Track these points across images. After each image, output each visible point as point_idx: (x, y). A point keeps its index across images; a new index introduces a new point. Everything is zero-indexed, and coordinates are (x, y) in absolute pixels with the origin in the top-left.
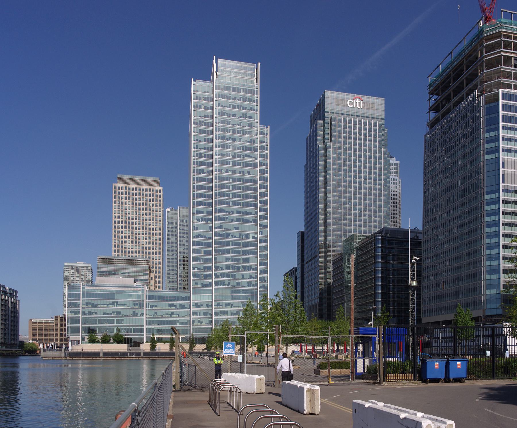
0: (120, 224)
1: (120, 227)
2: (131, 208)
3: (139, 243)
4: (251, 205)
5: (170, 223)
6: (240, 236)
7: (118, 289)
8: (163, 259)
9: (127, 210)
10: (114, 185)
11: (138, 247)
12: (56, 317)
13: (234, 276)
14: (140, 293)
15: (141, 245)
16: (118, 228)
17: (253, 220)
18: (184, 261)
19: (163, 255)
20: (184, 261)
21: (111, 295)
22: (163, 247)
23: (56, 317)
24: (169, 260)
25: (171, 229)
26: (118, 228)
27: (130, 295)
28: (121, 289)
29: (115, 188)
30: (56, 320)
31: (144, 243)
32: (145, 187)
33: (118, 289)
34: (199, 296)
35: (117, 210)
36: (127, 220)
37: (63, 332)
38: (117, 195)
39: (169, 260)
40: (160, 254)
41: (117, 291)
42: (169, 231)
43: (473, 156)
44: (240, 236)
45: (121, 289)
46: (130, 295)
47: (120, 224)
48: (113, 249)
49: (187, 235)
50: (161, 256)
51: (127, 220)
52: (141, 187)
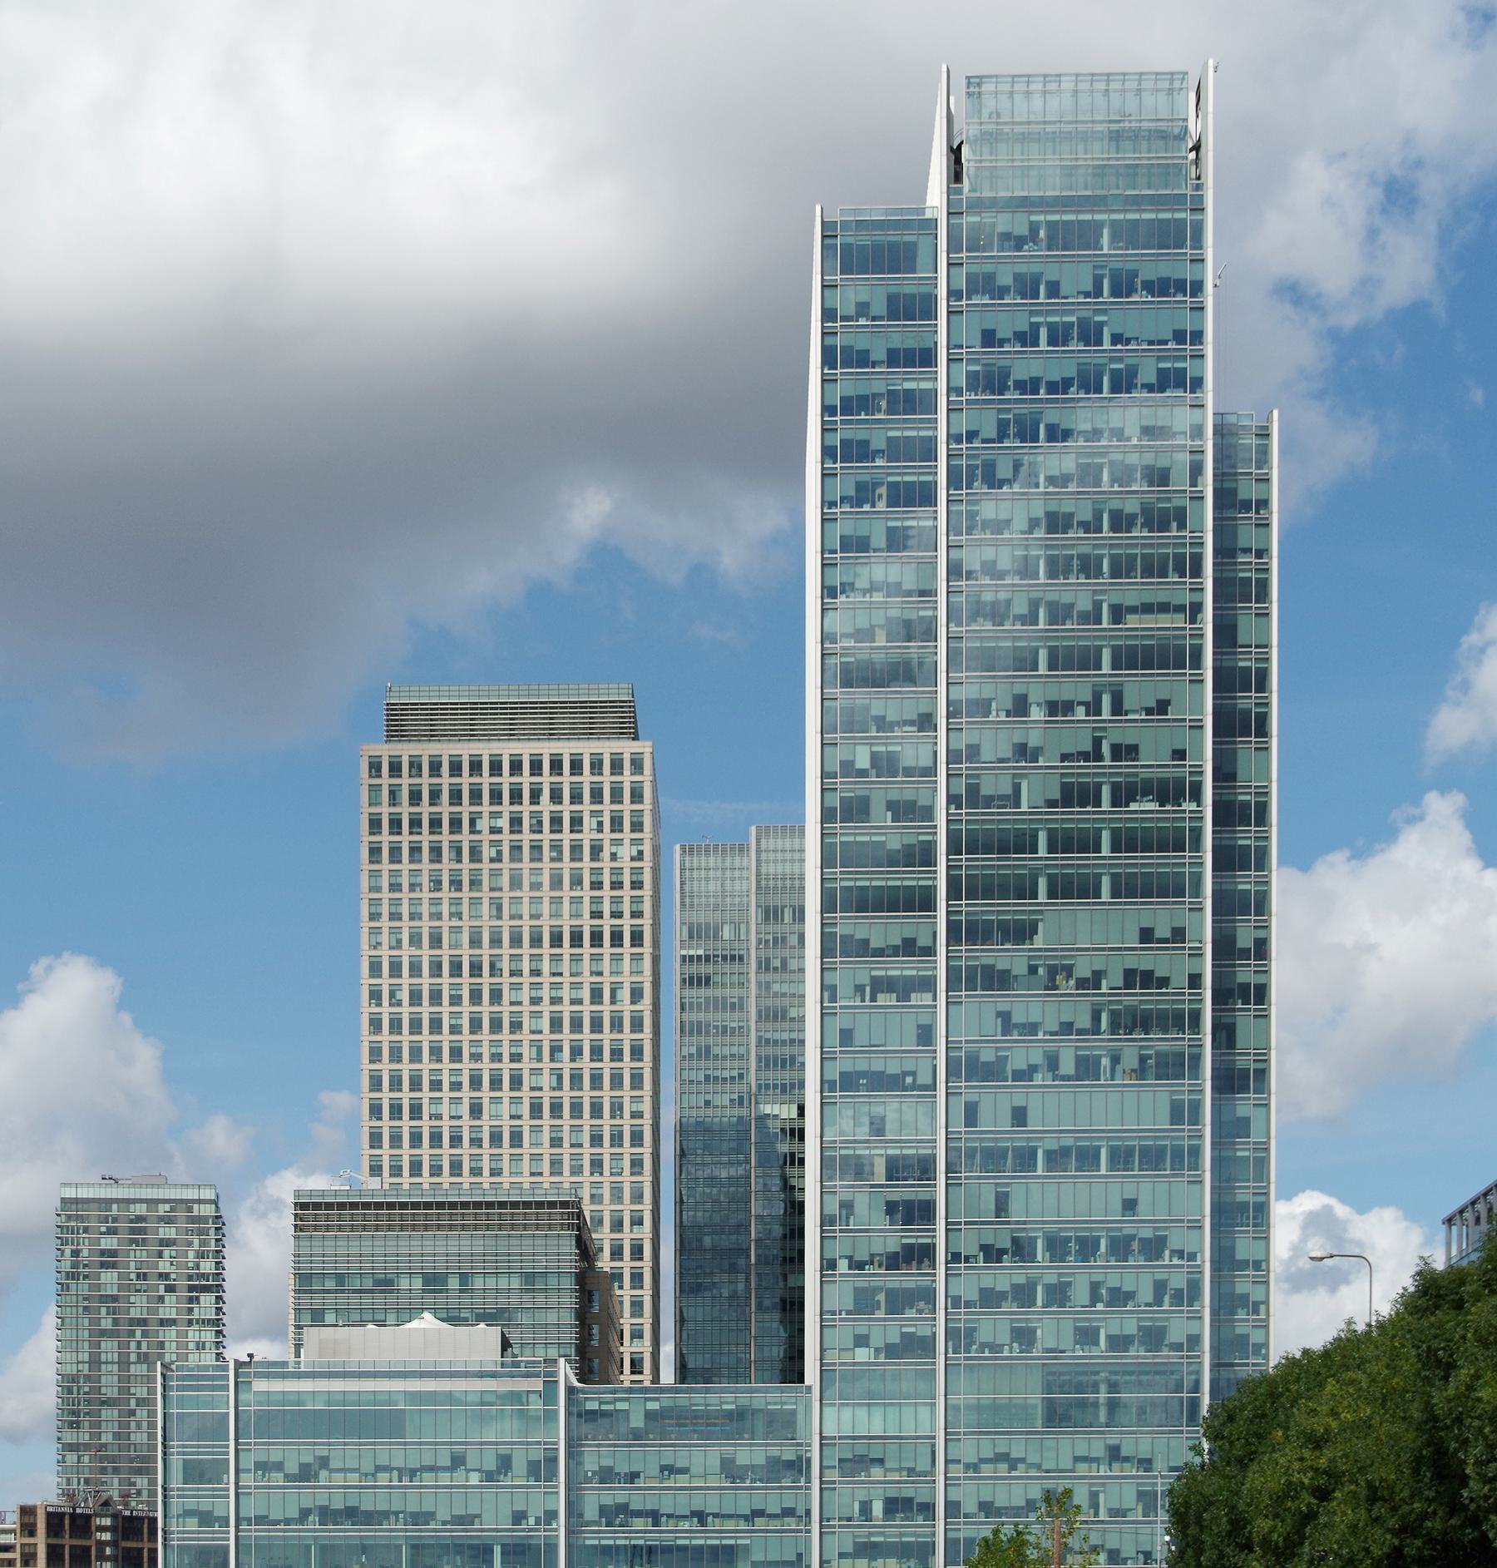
0: (406, 980)
1: (404, 996)
3: (516, 1082)
5: (694, 933)
6: (1096, 1018)
8: (656, 960)
11: (505, 1109)
12: (27, 1512)
15: (525, 1093)
16: (395, 1002)
17: (1179, 560)
18: (775, 1065)
19: (656, 944)
20: (775, 1065)
22: (656, 926)
23: (27, 1512)
24: (695, 969)
25: (703, 969)
26: (395, 1002)
28: (429, 1385)
29: (375, 767)
30: (29, 1529)
31: (546, 1080)
32: (546, 749)
35: (386, 895)
37: (67, 1541)
38: (385, 1037)
39: (695, 969)
40: (637, 938)
42: (691, 981)
44: (1096, 1018)
45: (429, 1385)
47: (406, 980)
48: (367, 1009)
50: (647, 949)
52: (525, 749)
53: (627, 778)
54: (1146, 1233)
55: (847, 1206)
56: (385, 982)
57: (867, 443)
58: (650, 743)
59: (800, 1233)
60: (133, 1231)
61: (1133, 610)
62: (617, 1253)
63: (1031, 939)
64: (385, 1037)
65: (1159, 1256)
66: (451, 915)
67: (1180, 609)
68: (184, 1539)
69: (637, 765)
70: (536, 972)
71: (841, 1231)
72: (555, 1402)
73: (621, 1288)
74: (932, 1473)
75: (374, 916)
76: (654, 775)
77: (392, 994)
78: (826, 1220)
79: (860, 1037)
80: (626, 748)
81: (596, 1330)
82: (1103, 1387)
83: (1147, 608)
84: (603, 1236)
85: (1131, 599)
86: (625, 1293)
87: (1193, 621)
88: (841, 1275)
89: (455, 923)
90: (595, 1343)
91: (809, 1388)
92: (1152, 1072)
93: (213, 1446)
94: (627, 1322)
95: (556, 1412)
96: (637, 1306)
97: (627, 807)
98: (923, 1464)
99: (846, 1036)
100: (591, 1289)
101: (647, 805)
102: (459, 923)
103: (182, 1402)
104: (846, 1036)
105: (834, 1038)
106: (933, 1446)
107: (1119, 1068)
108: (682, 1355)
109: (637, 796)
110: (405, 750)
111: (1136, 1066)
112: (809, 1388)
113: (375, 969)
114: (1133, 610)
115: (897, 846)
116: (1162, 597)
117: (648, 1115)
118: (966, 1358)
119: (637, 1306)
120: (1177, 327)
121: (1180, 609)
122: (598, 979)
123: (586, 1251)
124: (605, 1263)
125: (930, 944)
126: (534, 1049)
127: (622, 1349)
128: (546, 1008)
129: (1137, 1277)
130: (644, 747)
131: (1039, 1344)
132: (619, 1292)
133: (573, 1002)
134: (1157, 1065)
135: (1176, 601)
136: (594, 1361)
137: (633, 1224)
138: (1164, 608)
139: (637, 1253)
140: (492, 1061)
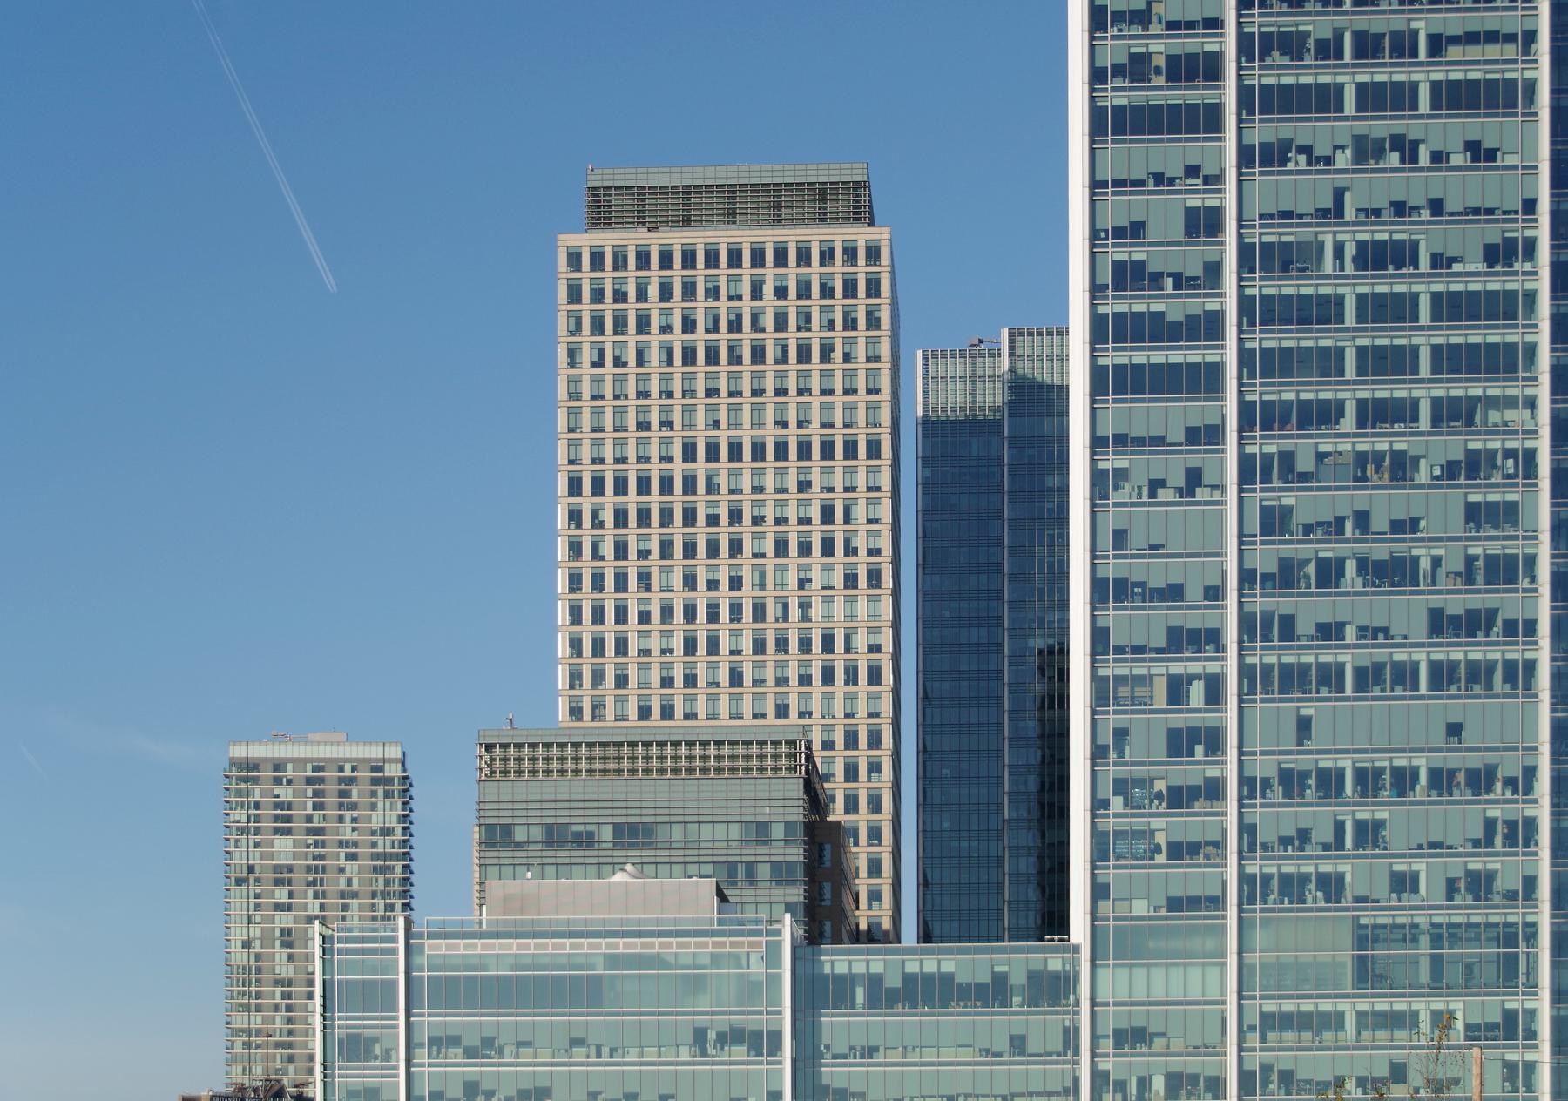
0: (609, 500)
2: (677, 388)
4: (1277, 364)
7: (621, 946)
9: (654, 402)
10: (567, 240)
13: (1369, 834)
14: (757, 969)
21: (583, 990)
27: (696, 984)
28: (637, 946)
29: (574, 260)
33: (621, 946)
34: (1140, 973)
36: (678, 470)
38: (586, 308)
41: (613, 961)
43: (955, 424)
45: (637, 946)
46: (696, 984)
49: (1145, 498)
51: (678, 470)
53: (862, 270)
54: (1475, 760)
55: (1121, 734)
56: (586, 502)
57: (1143, 263)
58: (888, 230)
59: (1063, 701)
60: (289, 819)
61: (1455, 40)
62: (851, 805)
63: (1337, 423)
64: (586, 308)
65: (1489, 789)
66: (662, 424)
67: (1510, 38)
68: (347, 1076)
69: (873, 254)
70: (757, 393)
71: (1113, 38)
72: (779, 965)
73: (856, 844)
74: (1223, 1043)
75: (575, 395)
76: (893, 266)
77: (594, 515)
78: (1098, 752)
79: (1137, 540)
80: (860, 235)
81: (827, 888)
82: (1425, 940)
83: (1472, 38)
84: (837, 788)
85: (1455, 30)
86: (860, 854)
87: (1526, 52)
88: (1116, 815)
89: (666, 433)
90: (827, 903)
91: (1077, 949)
92: (1480, 578)
93: (382, 1018)
94: (863, 884)
95: (779, 977)
96: (875, 868)
97: (862, 302)
98: (1213, 1037)
99: (1120, 537)
100: (822, 844)
101: (884, 300)
102: (670, 434)
103: (346, 967)
104: (1120, 537)
105: (1106, 541)
106: (1223, 1012)
107: (1441, 572)
108: (925, 923)
109: (873, 288)
110: (608, 240)
111: (1461, 568)
112: (1077, 949)
113: (575, 486)
114: (1455, 40)
115: (1180, 317)
116: (1490, 26)
117: (887, 551)
118: (1262, 910)
119: (875, 868)
120: (1528, 873)
121: (1510, 38)
122: (830, 495)
123: (816, 800)
124: (837, 813)
125: (1219, 583)
126: (757, 574)
127: (857, 913)
128: (769, 528)
129: (1462, 816)
130: (881, 234)
131: (1348, 893)
132: (854, 849)
133: (801, 522)
134: (1486, 565)
135: (1506, 30)
136: (825, 917)
137: (870, 771)
138: (1492, 37)
139: (875, 804)
140: (708, 524)
